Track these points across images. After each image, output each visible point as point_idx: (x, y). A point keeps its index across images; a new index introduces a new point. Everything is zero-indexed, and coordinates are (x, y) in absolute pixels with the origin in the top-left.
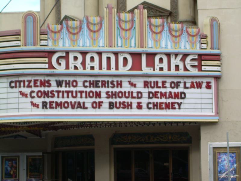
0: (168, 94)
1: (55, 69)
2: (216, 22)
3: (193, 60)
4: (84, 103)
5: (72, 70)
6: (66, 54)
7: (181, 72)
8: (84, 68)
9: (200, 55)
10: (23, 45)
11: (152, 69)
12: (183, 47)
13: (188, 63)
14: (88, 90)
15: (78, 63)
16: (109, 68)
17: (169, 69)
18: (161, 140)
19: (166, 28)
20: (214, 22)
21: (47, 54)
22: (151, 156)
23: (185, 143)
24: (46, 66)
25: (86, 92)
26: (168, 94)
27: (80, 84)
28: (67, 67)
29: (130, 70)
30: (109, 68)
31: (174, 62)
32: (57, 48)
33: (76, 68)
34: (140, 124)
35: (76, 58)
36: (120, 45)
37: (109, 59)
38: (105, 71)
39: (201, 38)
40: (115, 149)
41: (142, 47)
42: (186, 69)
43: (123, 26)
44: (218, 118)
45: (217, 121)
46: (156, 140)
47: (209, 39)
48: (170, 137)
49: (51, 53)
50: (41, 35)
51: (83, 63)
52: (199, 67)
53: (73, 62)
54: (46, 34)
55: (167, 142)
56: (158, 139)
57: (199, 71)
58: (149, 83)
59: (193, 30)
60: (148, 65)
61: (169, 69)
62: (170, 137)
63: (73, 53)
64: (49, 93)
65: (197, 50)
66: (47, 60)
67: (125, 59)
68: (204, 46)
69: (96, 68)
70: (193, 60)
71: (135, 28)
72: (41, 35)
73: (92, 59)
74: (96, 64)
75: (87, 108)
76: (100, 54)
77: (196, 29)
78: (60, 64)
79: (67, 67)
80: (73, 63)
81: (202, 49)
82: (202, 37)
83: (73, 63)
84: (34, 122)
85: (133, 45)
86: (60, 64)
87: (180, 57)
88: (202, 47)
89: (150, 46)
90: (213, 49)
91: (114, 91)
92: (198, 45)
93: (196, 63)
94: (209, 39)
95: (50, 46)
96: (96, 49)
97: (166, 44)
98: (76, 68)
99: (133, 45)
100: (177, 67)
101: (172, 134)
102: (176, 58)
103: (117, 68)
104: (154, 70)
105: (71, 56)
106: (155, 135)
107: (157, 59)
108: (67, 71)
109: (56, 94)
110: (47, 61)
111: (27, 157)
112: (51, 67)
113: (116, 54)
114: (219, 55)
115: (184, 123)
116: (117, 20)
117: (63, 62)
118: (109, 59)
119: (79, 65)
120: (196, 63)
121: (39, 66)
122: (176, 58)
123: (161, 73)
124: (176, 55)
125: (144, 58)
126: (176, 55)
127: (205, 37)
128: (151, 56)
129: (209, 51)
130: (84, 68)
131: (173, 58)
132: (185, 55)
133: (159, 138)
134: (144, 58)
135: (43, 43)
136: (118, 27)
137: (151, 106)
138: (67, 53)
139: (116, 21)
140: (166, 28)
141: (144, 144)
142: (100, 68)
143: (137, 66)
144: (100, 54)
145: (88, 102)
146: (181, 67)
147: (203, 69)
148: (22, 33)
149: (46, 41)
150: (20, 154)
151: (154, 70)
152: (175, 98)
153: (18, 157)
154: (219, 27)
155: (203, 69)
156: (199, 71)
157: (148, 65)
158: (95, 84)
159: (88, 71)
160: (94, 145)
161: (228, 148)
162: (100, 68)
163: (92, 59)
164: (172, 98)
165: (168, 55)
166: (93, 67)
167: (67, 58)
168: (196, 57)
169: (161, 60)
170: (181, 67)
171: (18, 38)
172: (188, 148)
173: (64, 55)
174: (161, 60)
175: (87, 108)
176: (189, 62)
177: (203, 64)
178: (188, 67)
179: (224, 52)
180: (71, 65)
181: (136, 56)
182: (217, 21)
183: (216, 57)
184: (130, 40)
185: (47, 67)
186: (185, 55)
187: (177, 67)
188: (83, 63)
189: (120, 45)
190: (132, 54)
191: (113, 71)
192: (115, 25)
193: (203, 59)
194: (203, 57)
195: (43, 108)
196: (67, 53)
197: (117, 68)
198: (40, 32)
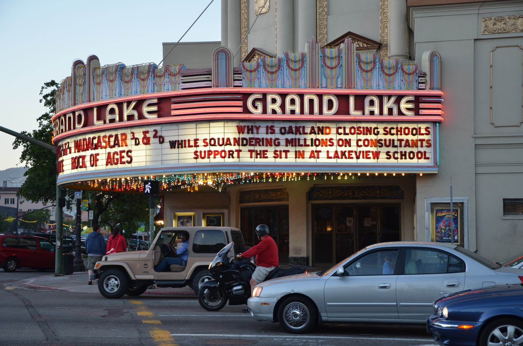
8: (284, 112)
15: (276, 107)
16: (311, 112)
18: (368, 194)
24: (240, 110)
28: (265, 111)
29: (336, 114)
37: (311, 101)
39: (419, 77)
41: (350, 88)
42: (400, 113)
46: (361, 194)
47: (428, 78)
48: (378, 192)
49: (246, 95)
51: (283, 107)
54: (241, 74)
59: (409, 67)
60: (356, 109)
62: (378, 192)
66: (241, 103)
68: (422, 86)
78: (256, 108)
79: (265, 111)
86: (256, 108)
87: (393, 99)
88: (420, 88)
92: (415, 84)
93: (410, 106)
100: (390, 111)
104: (364, 114)
105: (269, 98)
107: (367, 101)
110: (242, 105)
112: (246, 111)
117: (259, 105)
118: (311, 101)
119: (279, 110)
125: (352, 100)
126: (390, 97)
127: (424, 75)
130: (284, 112)
131: (385, 99)
132: (140, 103)
135: (237, 83)
138: (265, 95)
139: (320, 58)
142: (302, 112)
146: (395, 111)
149: (241, 82)
155: (420, 113)
157: (356, 109)
160: (288, 200)
165: (380, 97)
167: (264, 100)
170: (395, 111)
180: (269, 111)
181: (343, 98)
185: (242, 111)
188: (283, 107)
190: (339, 96)
191: (316, 116)
197: (321, 112)
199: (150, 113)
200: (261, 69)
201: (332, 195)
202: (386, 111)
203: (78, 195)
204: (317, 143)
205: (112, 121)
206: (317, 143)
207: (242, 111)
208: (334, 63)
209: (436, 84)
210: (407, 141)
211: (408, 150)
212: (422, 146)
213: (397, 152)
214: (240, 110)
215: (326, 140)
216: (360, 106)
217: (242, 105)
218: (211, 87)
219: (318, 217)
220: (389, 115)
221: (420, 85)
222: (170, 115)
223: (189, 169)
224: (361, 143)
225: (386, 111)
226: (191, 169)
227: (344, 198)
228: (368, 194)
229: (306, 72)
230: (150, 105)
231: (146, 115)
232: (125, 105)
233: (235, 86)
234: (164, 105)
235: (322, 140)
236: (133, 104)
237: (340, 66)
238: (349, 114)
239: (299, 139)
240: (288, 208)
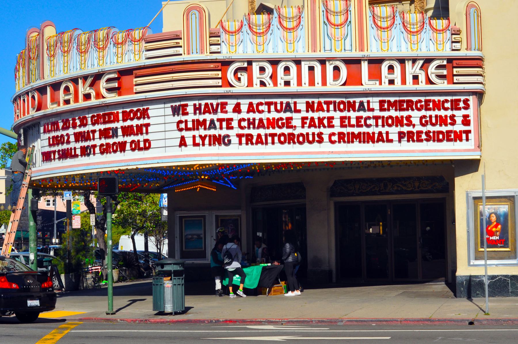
0: (257, 122)
1: (231, 86)
2: (474, 9)
3: (439, 67)
4: (387, 133)
5: (257, 88)
6: (248, 65)
7: (423, 86)
8: (275, 84)
9: (450, 60)
10: (198, 51)
11: (378, 82)
12: (374, 50)
13: (432, 73)
14: (386, 114)
15: (266, 77)
16: (312, 82)
17: (404, 82)
18: (404, 188)
19: (398, 20)
20: (472, 10)
21: (220, 64)
22: (389, 213)
23: (438, 191)
25: (383, 117)
26: (257, 122)
27: (190, 109)
28: (250, 83)
30: (312, 82)
31: (410, 69)
32: (234, 56)
33: (263, 84)
34: (383, 166)
35: (262, 70)
36: (328, 47)
37: (311, 69)
38: (306, 88)
39: (452, 34)
40: (336, 204)
41: (362, 50)
42: (429, 82)
43: (332, 19)
44: (479, 153)
45: (478, 157)
46: (396, 188)
47: (463, 36)
48: (417, 184)
49: (226, 63)
50: (210, 37)
51: (274, 77)
52: (449, 78)
53: (259, 76)
54: (219, 36)
55: (412, 192)
56: (398, 186)
57: (448, 83)
58: (124, 110)
59: (440, 24)
61: (404, 82)
62: (417, 184)
63: (257, 63)
64: (404, 119)
65: (447, 51)
67: (336, 69)
68: (457, 46)
69: (256, 85)
70: (439, 67)
71: (350, 22)
72: (210, 37)
73: (287, 69)
74: (293, 77)
75: (391, 141)
76: (298, 62)
77: (444, 21)
79: (250, 83)
80: (258, 78)
81: (453, 50)
82: (453, 32)
83: (258, 78)
84: (208, 165)
85: (348, 47)
86: (239, 79)
88: (454, 48)
89: (374, 50)
90: (471, 50)
91: (271, 118)
92: (448, 45)
94: (463, 36)
95: (225, 53)
96: (292, 55)
97: (398, 45)
98: (263, 84)
99: (348, 47)
100: (416, 78)
101: (419, 179)
102: (413, 66)
103: (324, 83)
104: (381, 84)
105: (256, 67)
106: (394, 181)
108: (250, 90)
109: (217, 124)
111: (217, 217)
113: (323, 62)
114: (481, 59)
115: (352, 162)
116: (323, 11)
117: (244, 77)
118: (311, 69)
120: (445, 72)
121: (208, 84)
122: (413, 66)
123: (391, 88)
124: (414, 61)
125: (365, 66)
126: (414, 61)
127: (458, 32)
128: (375, 62)
129: (463, 53)
130: (275, 84)
131: (408, 65)
132: (428, 61)
133: (400, 185)
134: (365, 66)
135: (214, 48)
136: (324, 22)
137: (335, 138)
139: (321, 13)
140: (398, 20)
141: (378, 195)
142: (299, 83)
143: (354, 78)
144: (298, 62)
145: (394, 131)
146: (422, 78)
147: (455, 81)
148: (184, 36)
149: (219, 47)
150: (206, 213)
151: (381, 84)
152: (268, 128)
153: (204, 217)
154: (479, 16)
155: (455, 81)
156: (448, 83)
158: (398, 106)
159: (281, 88)
160: (305, 197)
161: (484, 199)
162: (299, 83)
163: (287, 69)
164: (264, 127)
165: (402, 61)
166: (259, 82)
167: (247, 69)
168: (445, 63)
169: (391, 68)
170: (422, 78)
171: (179, 43)
172: (444, 199)
173: (246, 65)
174: (391, 68)
175: (391, 141)
176: (433, 70)
177: (455, 73)
178: (433, 78)
179: (489, 53)
180: (256, 81)
181: (352, 63)
182: (475, 6)
183: (477, 62)
184: (343, 40)
186: (428, 61)
187: (416, 78)
188: (274, 77)
189: (328, 47)
190: (348, 62)
191: (318, 88)
192: (321, 18)
193: (455, 65)
194: (455, 62)
195: (247, 144)
196: (250, 63)
197: (324, 83)
198: (210, 33)
199: (109, 90)
200: (246, 28)
201: (419, 187)
202: (409, 79)
203: (68, 195)
204: (390, 121)
205: (67, 102)
206: (390, 121)
207: (220, 84)
208: (340, 19)
209: (474, 43)
210: (312, 119)
211: (254, 132)
212: (221, 128)
213: (334, 134)
214: (220, 82)
215: (402, 117)
216: (375, 76)
217: (220, 76)
218: (181, 55)
219: (348, 219)
220: (274, 86)
221: (454, 44)
222: (130, 91)
223: (156, 161)
224: (244, 124)
225: (409, 79)
226: (159, 161)
227: (375, 194)
228: (404, 188)
229: (303, 32)
230: (109, 81)
231: (103, 92)
232: (80, 81)
233: (211, 53)
234: (125, 79)
235: (397, 117)
236: (89, 81)
237: (348, 22)
238: (362, 85)
239: (349, 118)
240: (305, 208)
